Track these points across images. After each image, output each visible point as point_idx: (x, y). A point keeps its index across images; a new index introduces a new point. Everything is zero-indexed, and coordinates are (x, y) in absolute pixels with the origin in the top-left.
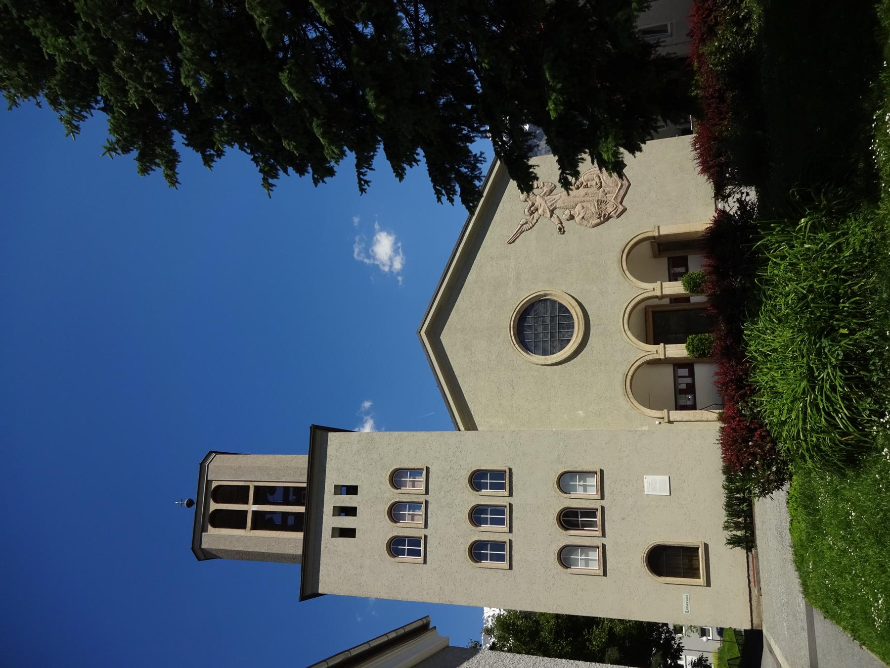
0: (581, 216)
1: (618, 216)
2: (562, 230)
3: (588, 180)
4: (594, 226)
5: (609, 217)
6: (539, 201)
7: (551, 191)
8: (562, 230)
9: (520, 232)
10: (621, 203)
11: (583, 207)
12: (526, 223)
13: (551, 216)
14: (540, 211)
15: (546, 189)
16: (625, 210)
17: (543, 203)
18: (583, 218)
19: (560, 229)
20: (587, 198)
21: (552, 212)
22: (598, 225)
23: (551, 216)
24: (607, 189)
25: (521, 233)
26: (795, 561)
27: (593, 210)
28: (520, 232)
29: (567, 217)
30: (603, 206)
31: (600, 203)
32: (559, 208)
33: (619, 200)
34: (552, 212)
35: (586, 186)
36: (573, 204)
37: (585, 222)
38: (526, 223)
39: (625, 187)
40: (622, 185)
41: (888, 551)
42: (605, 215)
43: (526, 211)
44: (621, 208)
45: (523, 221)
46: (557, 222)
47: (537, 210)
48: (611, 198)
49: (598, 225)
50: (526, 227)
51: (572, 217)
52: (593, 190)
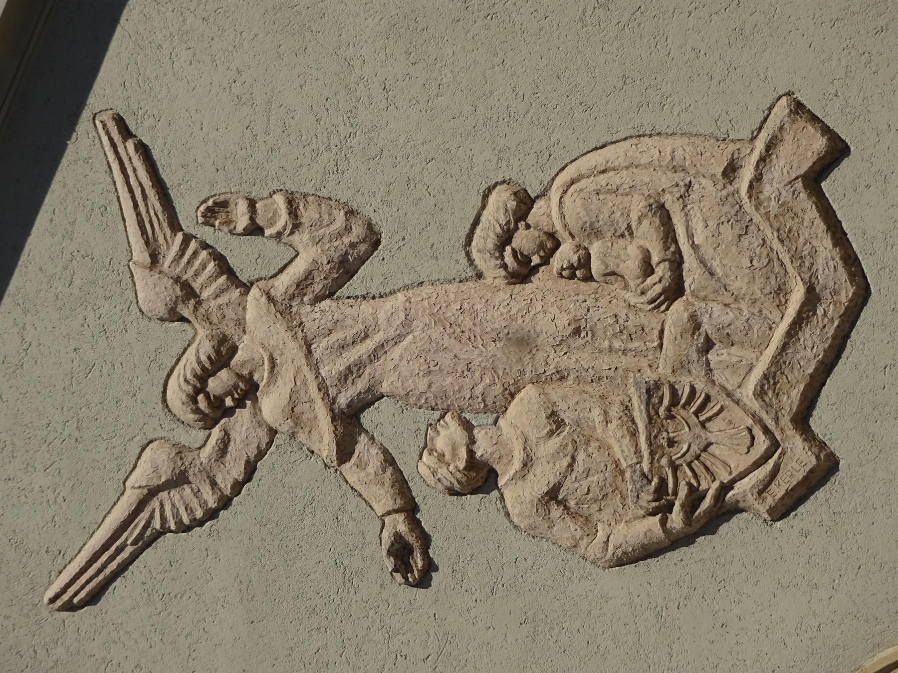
0: (542, 478)
1: (783, 510)
2: (412, 559)
3: (594, 232)
4: (624, 560)
5: (725, 511)
6: (260, 334)
7: (346, 269)
8: (412, 559)
9: (137, 538)
10: (802, 420)
11: (556, 422)
12: (179, 480)
13: (345, 452)
14: (271, 404)
15: (308, 255)
16: (826, 469)
17: (291, 354)
18: (553, 495)
19: (400, 552)
20: (579, 358)
21: (349, 423)
22: (648, 552)
23: (345, 452)
24: (715, 316)
25: (145, 542)
26: (728, 520)
27: (622, 450)
28: (137, 538)
29: (451, 474)
30: (687, 438)
31: (665, 404)
32: (405, 399)
33: (791, 399)
34: (349, 423)
35: (581, 271)
36: (489, 386)
37: (566, 529)
38: (179, 480)
39: (829, 312)
40: (812, 298)
41: (812, 672)
42: (695, 496)
43: (176, 394)
44: (799, 458)
45: (154, 464)
46: (383, 499)
47: (248, 391)
48: (740, 370)
49: (648, 552)
50: (174, 503)
51: (480, 477)
52: (629, 299)
